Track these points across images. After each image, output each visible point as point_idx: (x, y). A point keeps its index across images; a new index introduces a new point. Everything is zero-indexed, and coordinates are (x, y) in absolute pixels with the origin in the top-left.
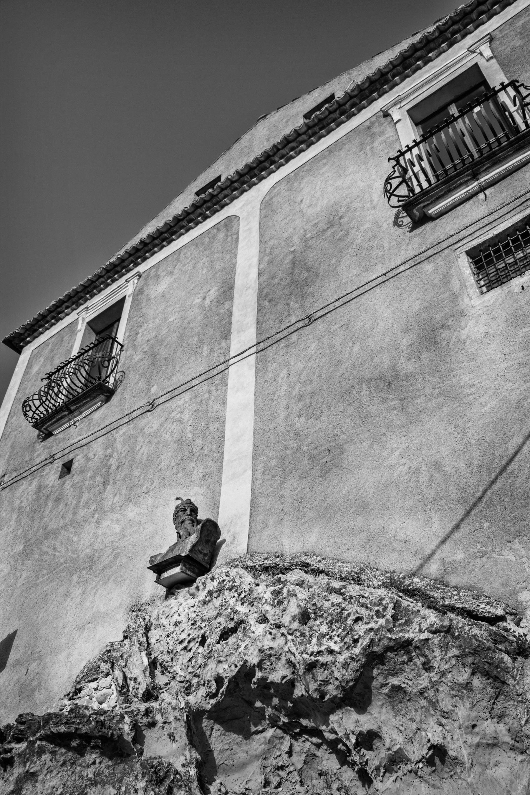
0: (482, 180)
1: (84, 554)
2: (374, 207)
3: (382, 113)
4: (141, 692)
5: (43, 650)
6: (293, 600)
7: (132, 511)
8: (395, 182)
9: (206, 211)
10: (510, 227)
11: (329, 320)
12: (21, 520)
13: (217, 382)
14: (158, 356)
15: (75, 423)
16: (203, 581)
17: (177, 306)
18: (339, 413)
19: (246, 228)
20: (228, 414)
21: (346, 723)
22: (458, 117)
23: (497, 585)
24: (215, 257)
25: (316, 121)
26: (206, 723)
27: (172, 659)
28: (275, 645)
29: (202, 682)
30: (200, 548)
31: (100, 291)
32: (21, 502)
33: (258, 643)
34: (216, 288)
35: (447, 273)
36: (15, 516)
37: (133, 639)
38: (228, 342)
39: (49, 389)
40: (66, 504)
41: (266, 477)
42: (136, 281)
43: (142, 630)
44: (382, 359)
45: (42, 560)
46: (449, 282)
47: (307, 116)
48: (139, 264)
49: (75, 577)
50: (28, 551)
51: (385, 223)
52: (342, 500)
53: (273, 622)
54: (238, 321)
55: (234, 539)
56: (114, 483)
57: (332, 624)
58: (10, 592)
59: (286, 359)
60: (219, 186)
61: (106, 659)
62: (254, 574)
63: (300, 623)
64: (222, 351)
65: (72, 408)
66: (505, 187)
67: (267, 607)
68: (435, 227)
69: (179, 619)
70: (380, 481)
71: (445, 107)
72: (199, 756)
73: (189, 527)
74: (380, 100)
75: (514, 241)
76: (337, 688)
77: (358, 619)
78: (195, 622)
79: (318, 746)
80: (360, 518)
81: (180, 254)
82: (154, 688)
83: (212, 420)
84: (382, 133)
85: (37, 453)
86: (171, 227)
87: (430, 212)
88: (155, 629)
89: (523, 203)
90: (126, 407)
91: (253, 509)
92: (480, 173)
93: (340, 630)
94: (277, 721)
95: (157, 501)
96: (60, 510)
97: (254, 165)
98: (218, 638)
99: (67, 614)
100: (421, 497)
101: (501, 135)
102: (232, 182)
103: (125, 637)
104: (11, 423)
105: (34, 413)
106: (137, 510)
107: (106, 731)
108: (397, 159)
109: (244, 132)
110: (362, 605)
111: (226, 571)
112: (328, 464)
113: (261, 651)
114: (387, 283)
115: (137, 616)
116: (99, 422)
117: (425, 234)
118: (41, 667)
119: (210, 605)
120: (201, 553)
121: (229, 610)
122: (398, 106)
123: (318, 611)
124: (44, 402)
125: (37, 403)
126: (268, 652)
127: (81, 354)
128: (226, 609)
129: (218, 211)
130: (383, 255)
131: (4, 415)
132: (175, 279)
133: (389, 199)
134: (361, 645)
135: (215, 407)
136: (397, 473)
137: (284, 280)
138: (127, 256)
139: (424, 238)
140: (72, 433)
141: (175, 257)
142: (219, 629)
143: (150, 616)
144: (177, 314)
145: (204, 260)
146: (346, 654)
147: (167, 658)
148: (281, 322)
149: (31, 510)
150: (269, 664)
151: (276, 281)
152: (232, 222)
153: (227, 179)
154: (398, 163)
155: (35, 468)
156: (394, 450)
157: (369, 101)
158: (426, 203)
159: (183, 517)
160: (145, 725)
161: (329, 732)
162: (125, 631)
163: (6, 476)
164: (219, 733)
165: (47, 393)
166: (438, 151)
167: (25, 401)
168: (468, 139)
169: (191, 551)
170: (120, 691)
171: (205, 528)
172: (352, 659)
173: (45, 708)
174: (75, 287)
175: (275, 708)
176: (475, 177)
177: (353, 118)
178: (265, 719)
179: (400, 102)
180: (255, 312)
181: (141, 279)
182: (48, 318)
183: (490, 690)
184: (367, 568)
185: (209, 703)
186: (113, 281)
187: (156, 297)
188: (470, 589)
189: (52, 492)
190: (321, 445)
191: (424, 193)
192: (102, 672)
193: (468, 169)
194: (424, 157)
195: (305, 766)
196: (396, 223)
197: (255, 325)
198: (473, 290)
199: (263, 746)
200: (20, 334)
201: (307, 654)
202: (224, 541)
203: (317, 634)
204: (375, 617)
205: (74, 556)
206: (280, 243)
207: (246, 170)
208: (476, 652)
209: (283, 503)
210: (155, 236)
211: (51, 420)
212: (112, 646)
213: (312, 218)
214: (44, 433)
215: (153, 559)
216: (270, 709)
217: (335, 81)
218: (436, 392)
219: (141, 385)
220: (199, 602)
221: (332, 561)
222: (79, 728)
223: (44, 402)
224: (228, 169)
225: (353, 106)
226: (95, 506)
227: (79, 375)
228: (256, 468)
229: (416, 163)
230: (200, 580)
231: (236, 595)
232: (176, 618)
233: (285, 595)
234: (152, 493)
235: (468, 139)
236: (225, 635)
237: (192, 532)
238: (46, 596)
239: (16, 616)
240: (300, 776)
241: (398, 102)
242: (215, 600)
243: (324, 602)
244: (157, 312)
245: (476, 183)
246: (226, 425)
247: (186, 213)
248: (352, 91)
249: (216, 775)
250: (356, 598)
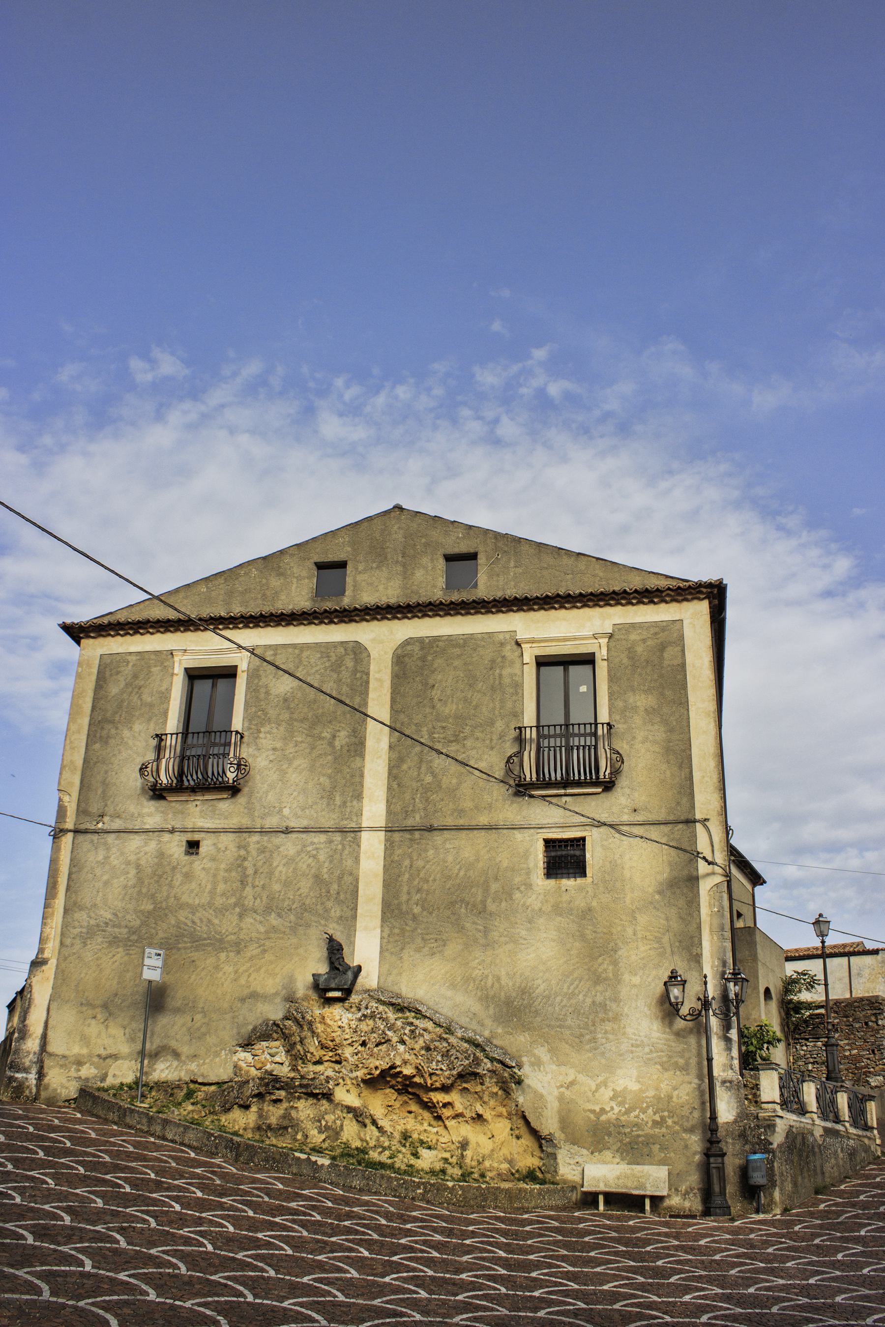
21: (438, 1097)
23: (514, 1050)
156: (476, 958)
176: (565, 787)
183: (504, 1096)
188: (502, 1048)
208: (503, 1082)
218: (506, 933)
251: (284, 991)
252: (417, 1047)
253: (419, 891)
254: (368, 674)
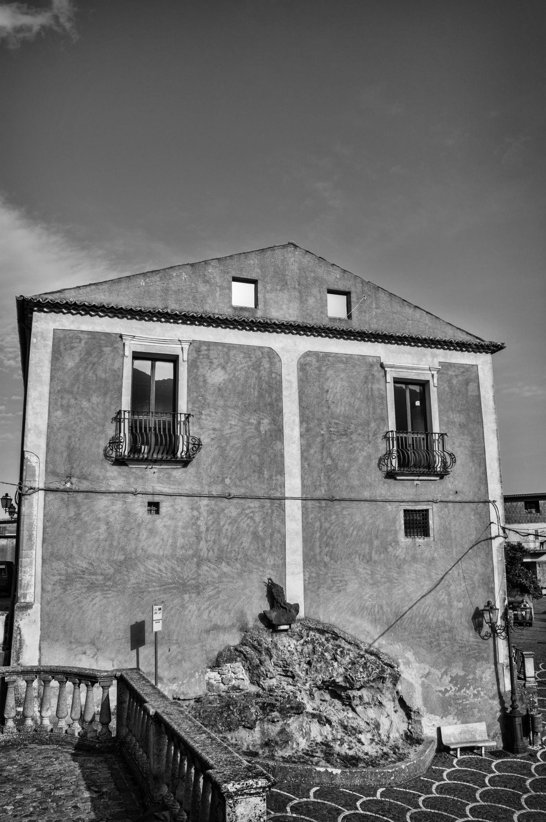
156: (367, 593)
176: (419, 476)
253: (327, 545)
254: (281, 375)
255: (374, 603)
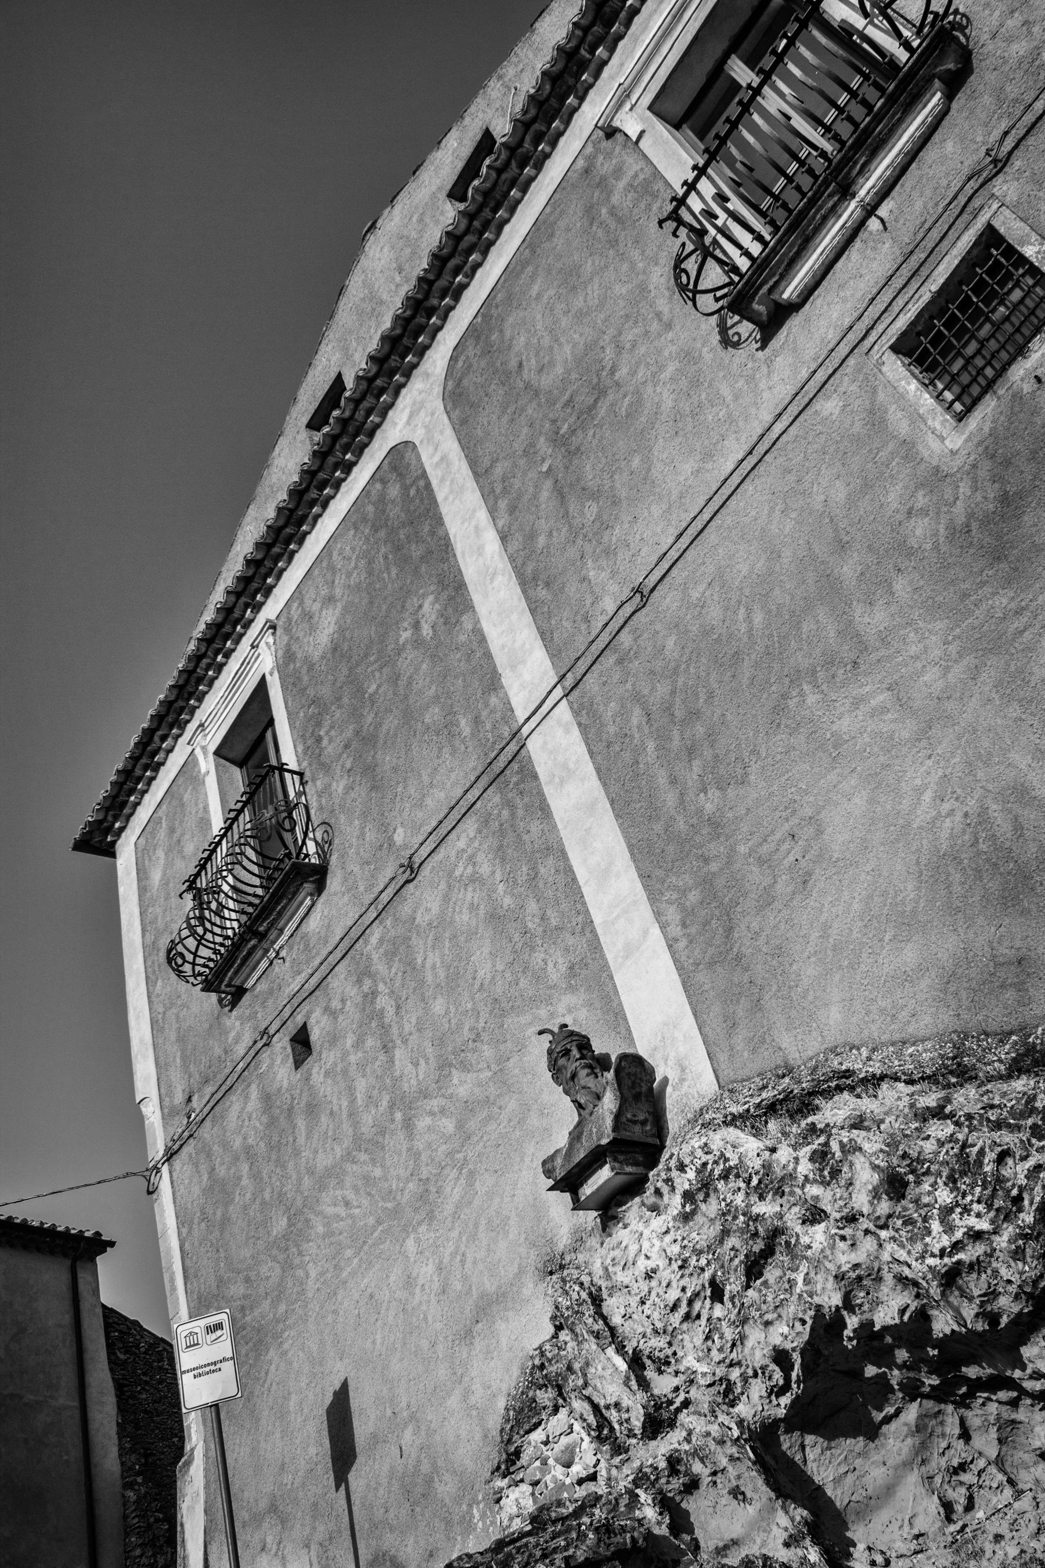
0: (862, 193)
1: (407, 1196)
2: (669, 326)
3: (601, 133)
4: (637, 1424)
5: (413, 1401)
6: (859, 1160)
7: (462, 1082)
8: (691, 265)
9: (345, 454)
10: (958, 266)
11: (679, 580)
12: (259, 1172)
13: (515, 779)
14: (378, 770)
15: (278, 953)
16: (663, 1175)
17: (372, 659)
18: (779, 757)
19: (436, 459)
20: (564, 834)
22: (761, 85)
24: (402, 537)
25: (479, 198)
26: (787, 1442)
27: (670, 1344)
28: (859, 1256)
29: (750, 1372)
30: (629, 1116)
31: (210, 685)
32: (245, 1138)
33: (827, 1263)
34: (431, 598)
35: (872, 403)
36: (245, 1168)
37: (578, 1330)
38: (501, 695)
39: (202, 909)
40: (331, 1113)
41: (693, 930)
42: (271, 640)
43: (589, 1310)
44: (818, 621)
45: (333, 1234)
46: (883, 421)
47: (457, 193)
48: (261, 604)
49: (410, 1244)
50: (299, 1225)
51: (705, 350)
52: (860, 924)
53: (838, 1216)
54: (503, 647)
55: (683, 1070)
56: (405, 1042)
57: (955, 1182)
58: (301, 1312)
59: (629, 686)
60: (348, 399)
61: (541, 1381)
62: (753, 1127)
63: (891, 1199)
64: (498, 715)
65: (261, 929)
66: (913, 188)
67: (813, 1190)
68: (808, 320)
69: (651, 1264)
70: (918, 863)
71: (719, 69)
72: (805, 1513)
73: (590, 1082)
74: (585, 107)
75: (976, 290)
76: (1017, 1297)
77: (1002, 1158)
78: (685, 1261)
79: (1014, 1404)
80: (910, 946)
81: (330, 555)
82: (658, 1407)
83: (538, 855)
84: (618, 172)
85: (232, 1034)
86: (292, 511)
87: (785, 296)
88: (610, 1295)
89: (965, 207)
90: (362, 889)
91: (694, 999)
92: (853, 182)
93: (978, 1189)
94: (919, 1387)
95: (502, 1047)
96: (324, 1127)
97: (398, 331)
98: (743, 1278)
99: (425, 1318)
100: (1011, 865)
101: (855, 82)
102: (370, 380)
103: (559, 1328)
104: (158, 996)
105: (194, 964)
106: (470, 1077)
107: (619, 1539)
108: (674, 216)
109: (347, 272)
110: (998, 1125)
111: (701, 1143)
112: (803, 863)
113: (839, 1277)
114: (761, 468)
115: (564, 1280)
116: (323, 934)
117: (795, 341)
118: (423, 1433)
119: (699, 1219)
120: (635, 1122)
121: (742, 1218)
122: (628, 106)
123: (917, 1165)
124: (202, 937)
125: (191, 943)
126: (853, 1275)
127: (230, 824)
128: (735, 1218)
129: (366, 445)
130: (730, 415)
131: (138, 984)
132: (345, 608)
133: (694, 300)
134: (1031, 1203)
135: (533, 829)
136: (945, 834)
137: (555, 534)
138: (233, 598)
139: (795, 350)
140: (280, 975)
141: (324, 564)
142: (737, 1261)
143: (590, 1274)
144: (377, 674)
145: (383, 550)
146: (1008, 1231)
147: (658, 1343)
148: (587, 620)
149: (270, 1147)
150: (862, 1294)
151: (542, 541)
152: (403, 457)
153: (358, 378)
154: (680, 222)
155: (241, 1065)
156: (920, 791)
157: (565, 117)
158: (771, 283)
159: (572, 1067)
160: (680, 1492)
161: (1031, 1377)
162: (554, 1318)
163: (195, 1098)
164: (818, 1450)
165: (201, 919)
166: (751, 170)
167: (169, 951)
168: (800, 123)
169: (616, 1128)
170: (598, 1437)
171: (623, 1074)
172: (1025, 1237)
173: (464, 1507)
174: (162, 696)
175: (903, 1366)
176: (846, 192)
177: (548, 163)
178: (892, 1391)
179: (628, 96)
180: (528, 617)
181: (278, 632)
182: (138, 772)
184: (966, 1037)
185: (779, 1405)
186: (227, 655)
187: (323, 657)
189: (293, 1099)
190: (773, 832)
191: (759, 265)
192: (544, 1408)
193: (826, 183)
194: (728, 193)
195: (1004, 1449)
196: (727, 342)
197: (539, 643)
198: (940, 420)
199: (909, 1441)
200: (99, 822)
201: (933, 1255)
202: (665, 1081)
203: (935, 1211)
204: (1034, 1141)
205: (389, 1205)
206: (515, 465)
207: (387, 348)
209: (747, 969)
210: (269, 541)
211: (231, 966)
212: (542, 1354)
213: (555, 392)
214: (228, 993)
215: (549, 1166)
216: (896, 1372)
217: (479, 102)
218: (953, 649)
219: (370, 836)
220: (674, 1219)
221: (891, 1049)
222: (570, 1557)
223: (202, 937)
224: (347, 356)
225: (537, 142)
226: (387, 1097)
227: (245, 863)
228: (664, 919)
229: (718, 211)
230: (656, 1176)
231: (743, 1185)
232: (643, 1265)
233: (838, 1155)
234: (485, 1037)
235: (800, 123)
236: (754, 1269)
237: (600, 1090)
238: (371, 1296)
239: (332, 1354)
240: (1002, 1470)
241: (624, 94)
242: (703, 1206)
243: (921, 1143)
244: (339, 684)
245: (853, 204)
246: (570, 855)
247: (309, 475)
248: (525, 112)
249: (848, 1529)
250: (981, 1116)
251: (533, 1253)
252: (861, 1201)
253: (691, 752)
255: (972, 804)
